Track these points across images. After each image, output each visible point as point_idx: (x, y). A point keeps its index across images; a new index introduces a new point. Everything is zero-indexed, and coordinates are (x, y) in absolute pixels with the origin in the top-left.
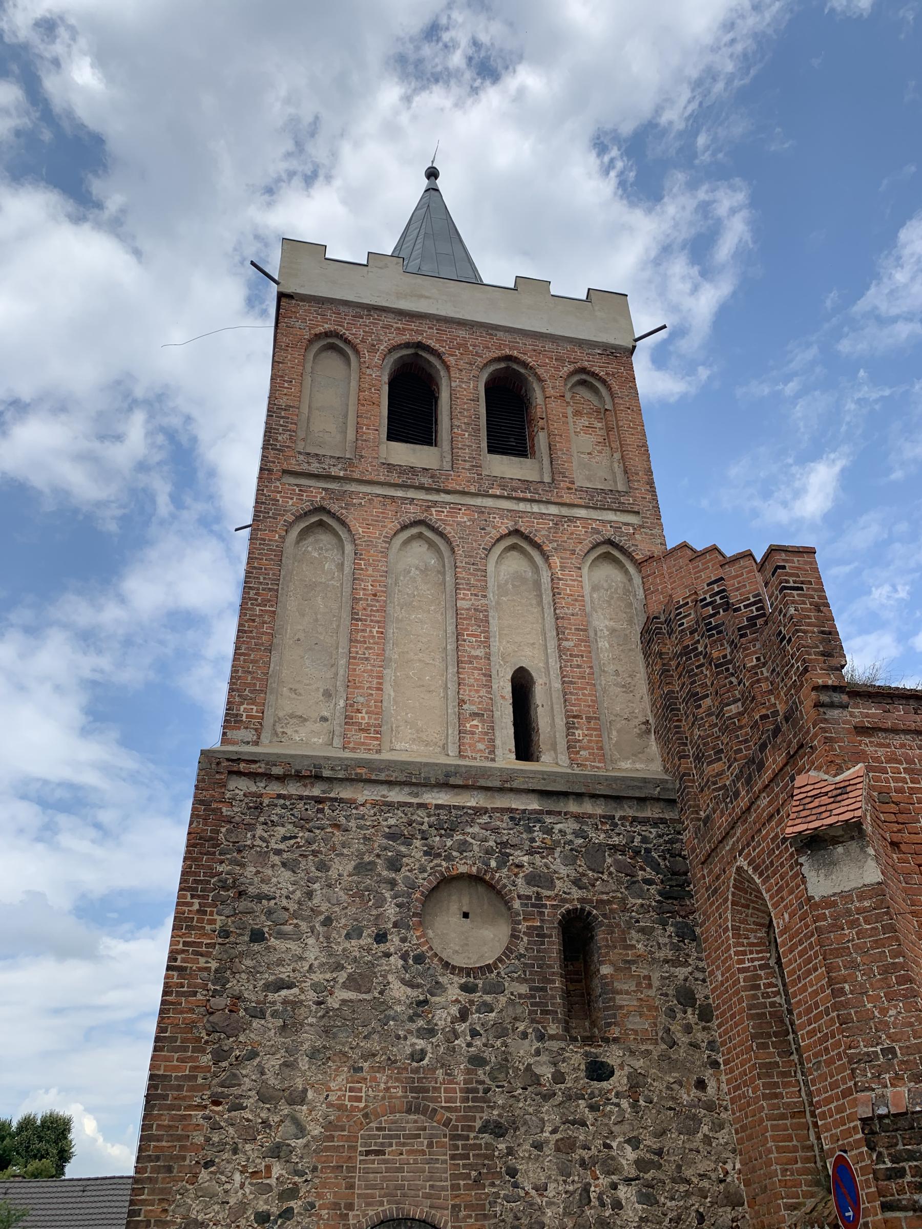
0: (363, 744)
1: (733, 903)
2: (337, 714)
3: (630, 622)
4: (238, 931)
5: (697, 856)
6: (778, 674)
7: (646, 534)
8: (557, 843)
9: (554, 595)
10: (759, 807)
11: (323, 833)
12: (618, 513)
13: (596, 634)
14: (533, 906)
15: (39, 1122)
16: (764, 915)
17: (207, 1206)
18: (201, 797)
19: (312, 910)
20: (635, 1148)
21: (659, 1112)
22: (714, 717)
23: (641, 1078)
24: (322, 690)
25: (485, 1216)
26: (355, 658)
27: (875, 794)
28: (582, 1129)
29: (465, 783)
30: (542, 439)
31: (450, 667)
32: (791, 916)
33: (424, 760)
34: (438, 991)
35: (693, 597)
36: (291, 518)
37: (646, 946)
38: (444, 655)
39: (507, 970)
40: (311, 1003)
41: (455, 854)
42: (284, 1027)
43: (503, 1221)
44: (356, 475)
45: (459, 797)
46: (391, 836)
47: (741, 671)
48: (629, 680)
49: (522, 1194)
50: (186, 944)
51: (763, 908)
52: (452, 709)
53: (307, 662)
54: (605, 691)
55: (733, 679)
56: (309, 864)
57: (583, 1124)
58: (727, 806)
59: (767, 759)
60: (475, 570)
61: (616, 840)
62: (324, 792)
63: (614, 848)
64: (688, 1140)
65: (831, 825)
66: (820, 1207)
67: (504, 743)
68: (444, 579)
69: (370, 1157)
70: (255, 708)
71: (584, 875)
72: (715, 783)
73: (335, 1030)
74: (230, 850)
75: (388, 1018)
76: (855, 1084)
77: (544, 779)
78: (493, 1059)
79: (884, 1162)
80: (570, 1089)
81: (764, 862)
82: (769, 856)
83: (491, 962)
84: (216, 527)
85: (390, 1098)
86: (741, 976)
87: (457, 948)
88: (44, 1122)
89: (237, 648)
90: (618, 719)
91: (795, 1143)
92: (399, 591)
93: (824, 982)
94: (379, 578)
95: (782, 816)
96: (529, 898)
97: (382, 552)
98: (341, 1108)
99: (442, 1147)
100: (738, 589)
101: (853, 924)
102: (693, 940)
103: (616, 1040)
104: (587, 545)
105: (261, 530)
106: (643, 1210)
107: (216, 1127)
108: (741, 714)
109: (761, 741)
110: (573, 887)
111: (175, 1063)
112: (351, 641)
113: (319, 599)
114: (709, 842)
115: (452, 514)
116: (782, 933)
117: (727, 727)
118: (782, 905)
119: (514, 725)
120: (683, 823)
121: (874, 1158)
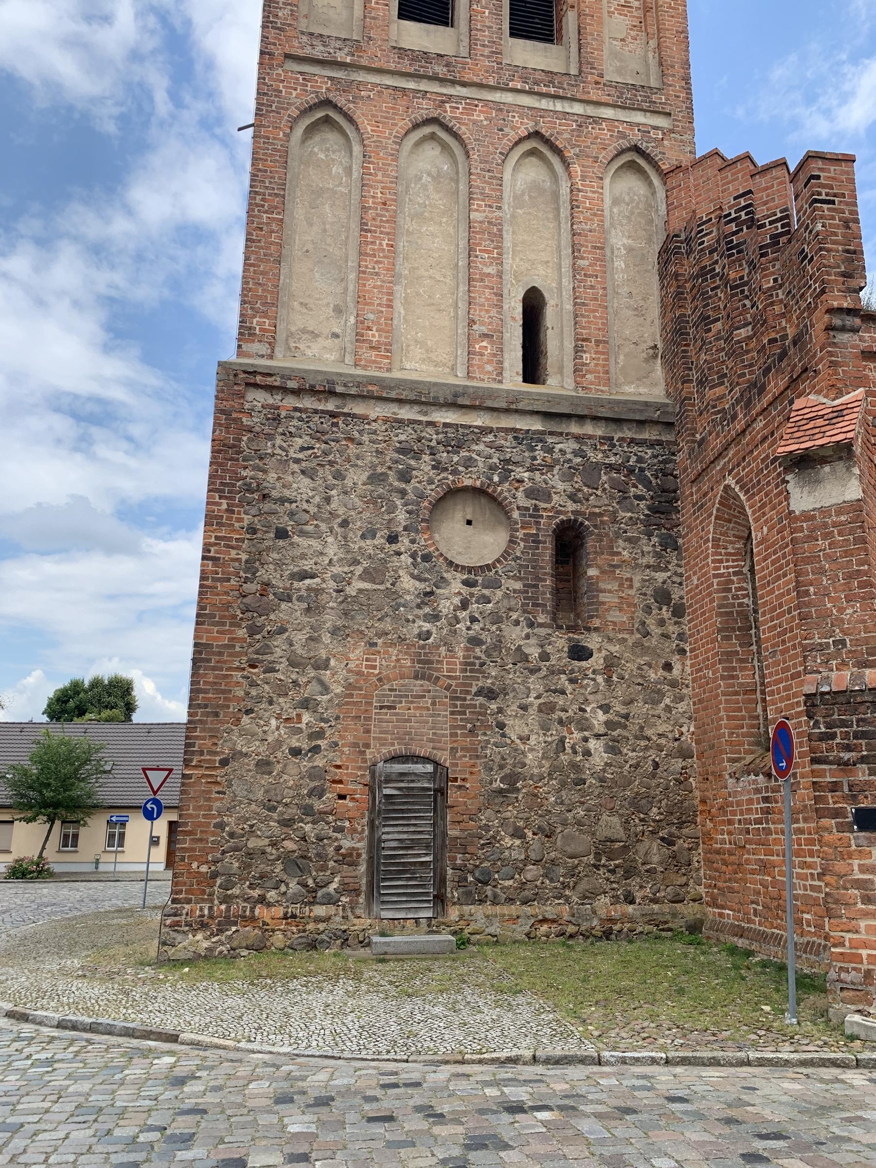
0: (374, 362)
1: (717, 518)
2: (349, 331)
3: (649, 241)
4: (264, 529)
5: (688, 476)
6: (794, 296)
7: (676, 140)
8: (556, 462)
9: (572, 208)
10: (754, 429)
11: (338, 445)
12: (648, 114)
13: (613, 253)
14: (531, 516)
15: (106, 682)
16: (744, 529)
17: (249, 742)
18: (222, 407)
19: (330, 513)
20: (606, 712)
21: (629, 687)
22: (722, 341)
23: (616, 660)
24: (332, 306)
25: (477, 757)
26: (364, 272)
27: (870, 418)
28: (561, 697)
29: (473, 403)
30: (570, 21)
31: (461, 285)
32: (769, 530)
33: (433, 380)
34: (443, 585)
35: (718, 212)
36: (295, 113)
37: (631, 553)
38: (455, 272)
39: (504, 570)
40: (331, 591)
41: (461, 468)
42: (308, 609)
43: (492, 760)
44: (364, 62)
45: (466, 417)
46: (402, 451)
47: (756, 293)
48: (642, 303)
49: (509, 741)
50: (217, 538)
51: (744, 523)
52: (462, 330)
53: (317, 275)
54: (616, 314)
55: (747, 302)
56: (326, 472)
57: (563, 692)
58: (723, 428)
59: (769, 383)
60: (491, 178)
61: (613, 460)
62: (338, 407)
63: (610, 467)
64: (652, 708)
65: (823, 445)
66: (758, 761)
67: (511, 366)
68: (458, 187)
69: (383, 711)
70: (267, 321)
71: (580, 490)
72: (714, 407)
73: (353, 613)
74: (253, 457)
75: (399, 605)
76: (806, 667)
77: (549, 401)
78: (489, 640)
79: (819, 728)
80: (553, 665)
81: (751, 480)
82: (757, 475)
83: (490, 562)
84: (218, 131)
85: (401, 667)
86: (715, 581)
87: (460, 550)
88: (110, 682)
89: (247, 258)
90: (627, 343)
91: (744, 713)
92: (410, 200)
93: (791, 586)
94: (388, 185)
95: (776, 438)
96: (527, 509)
97: (392, 155)
98: (359, 673)
99: (443, 705)
100: (765, 203)
101: (825, 537)
102: (675, 550)
103: (596, 629)
104: (612, 151)
105: (264, 126)
106: (608, 758)
107: (253, 684)
108: (749, 338)
109: (766, 365)
110: (568, 500)
111: (215, 634)
112: (360, 254)
113: (327, 207)
114: (701, 462)
115: (468, 111)
116: (758, 545)
117: (734, 352)
118: (763, 520)
119: (523, 347)
120: (679, 445)
121: (811, 724)
